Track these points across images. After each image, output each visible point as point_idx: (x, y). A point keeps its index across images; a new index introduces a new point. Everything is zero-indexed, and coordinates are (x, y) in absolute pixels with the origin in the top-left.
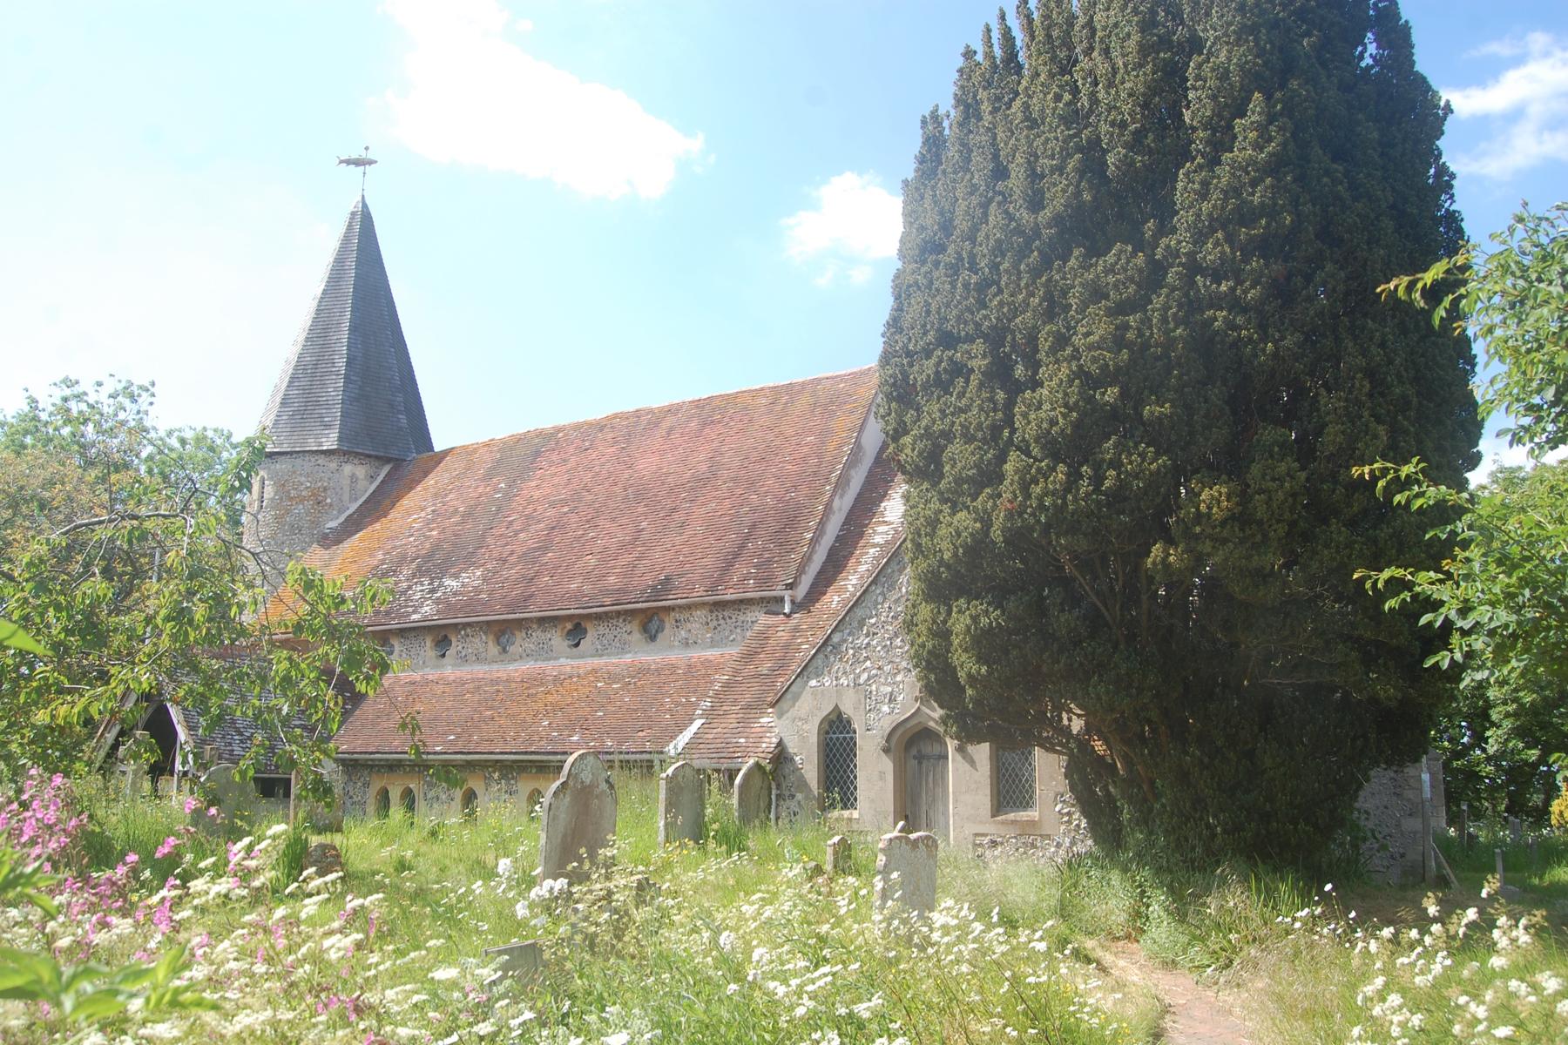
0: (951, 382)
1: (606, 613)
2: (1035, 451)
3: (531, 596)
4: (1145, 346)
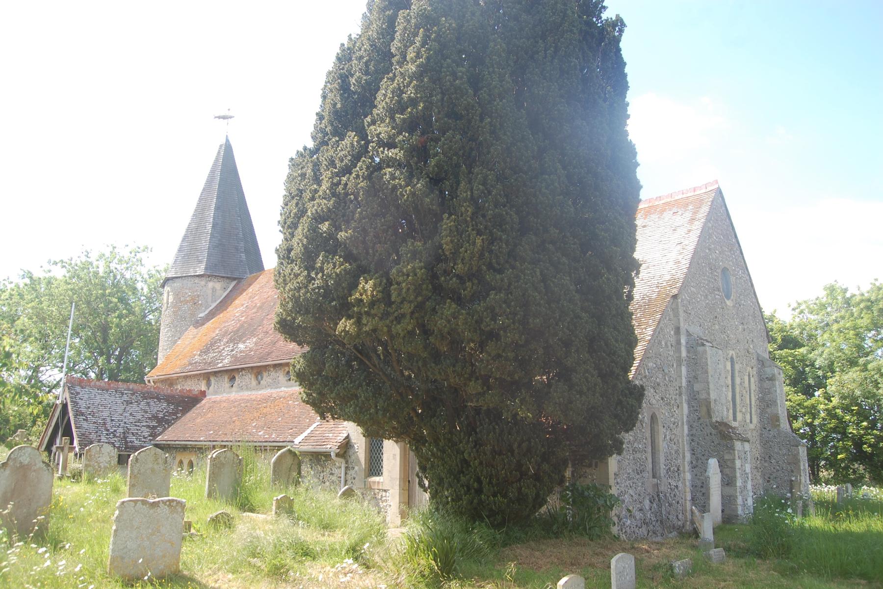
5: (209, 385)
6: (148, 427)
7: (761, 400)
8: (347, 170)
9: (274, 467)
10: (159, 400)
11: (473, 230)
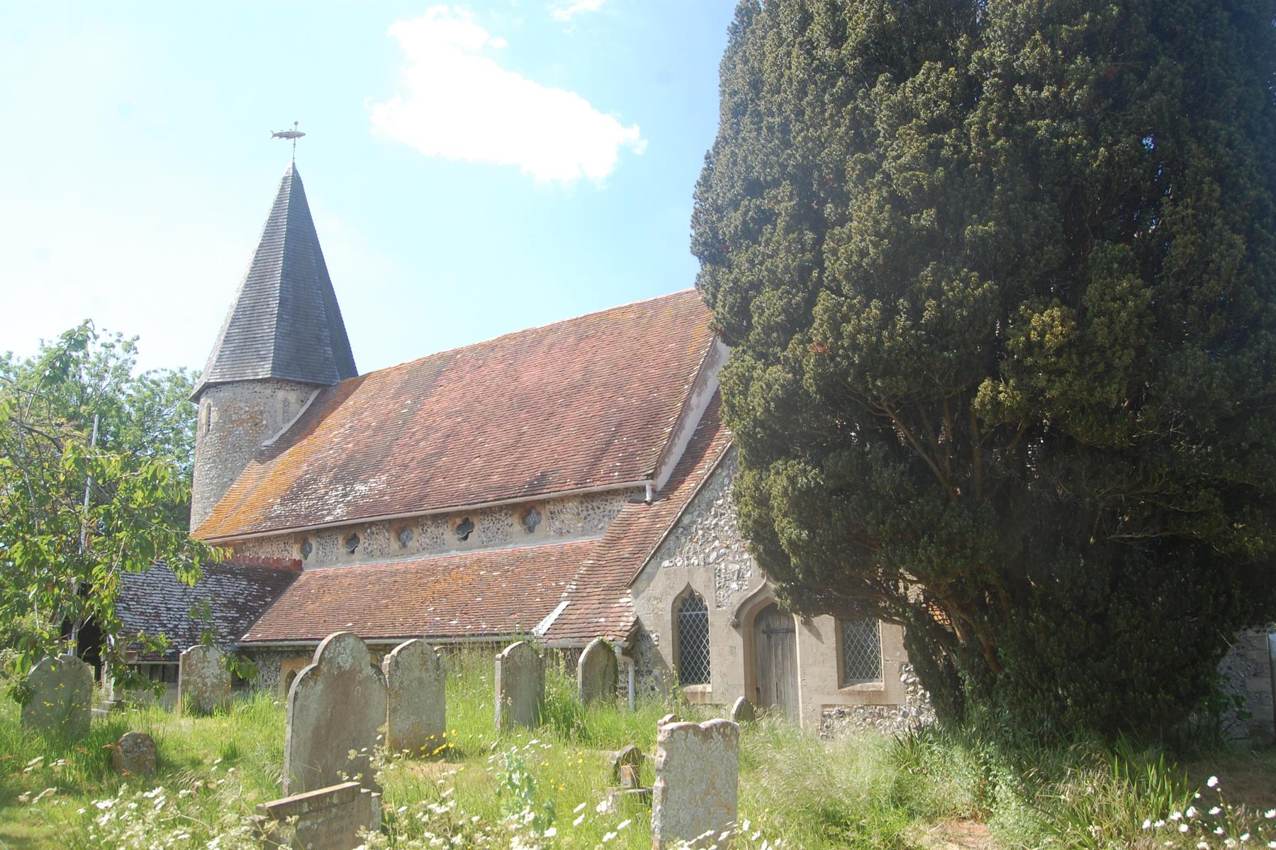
0: (760, 232)
1: (490, 508)
2: (846, 288)
3: (426, 496)
4: (963, 162)
6: (225, 619)
10: (235, 575)
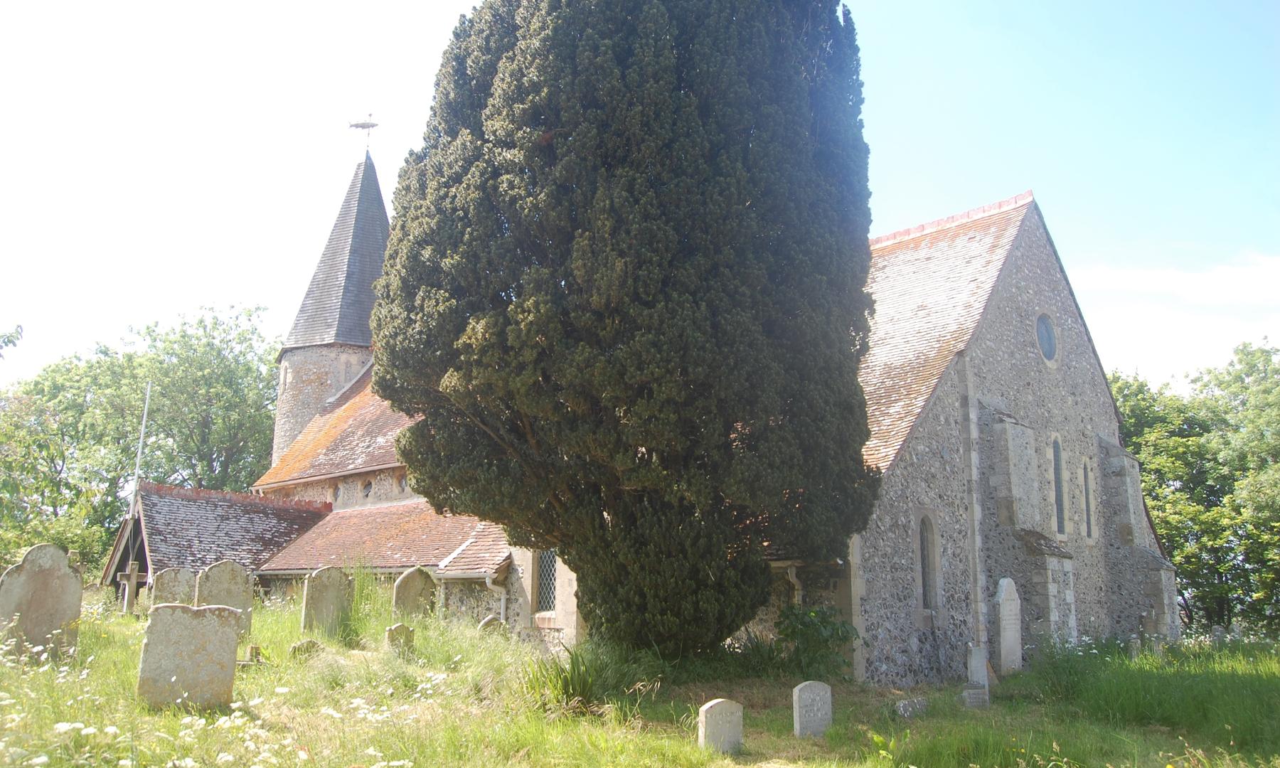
5: (336, 495)
6: (250, 551)
7: (1106, 504)
8: (457, 179)
9: (398, 593)
10: (266, 515)
11: (613, 250)
